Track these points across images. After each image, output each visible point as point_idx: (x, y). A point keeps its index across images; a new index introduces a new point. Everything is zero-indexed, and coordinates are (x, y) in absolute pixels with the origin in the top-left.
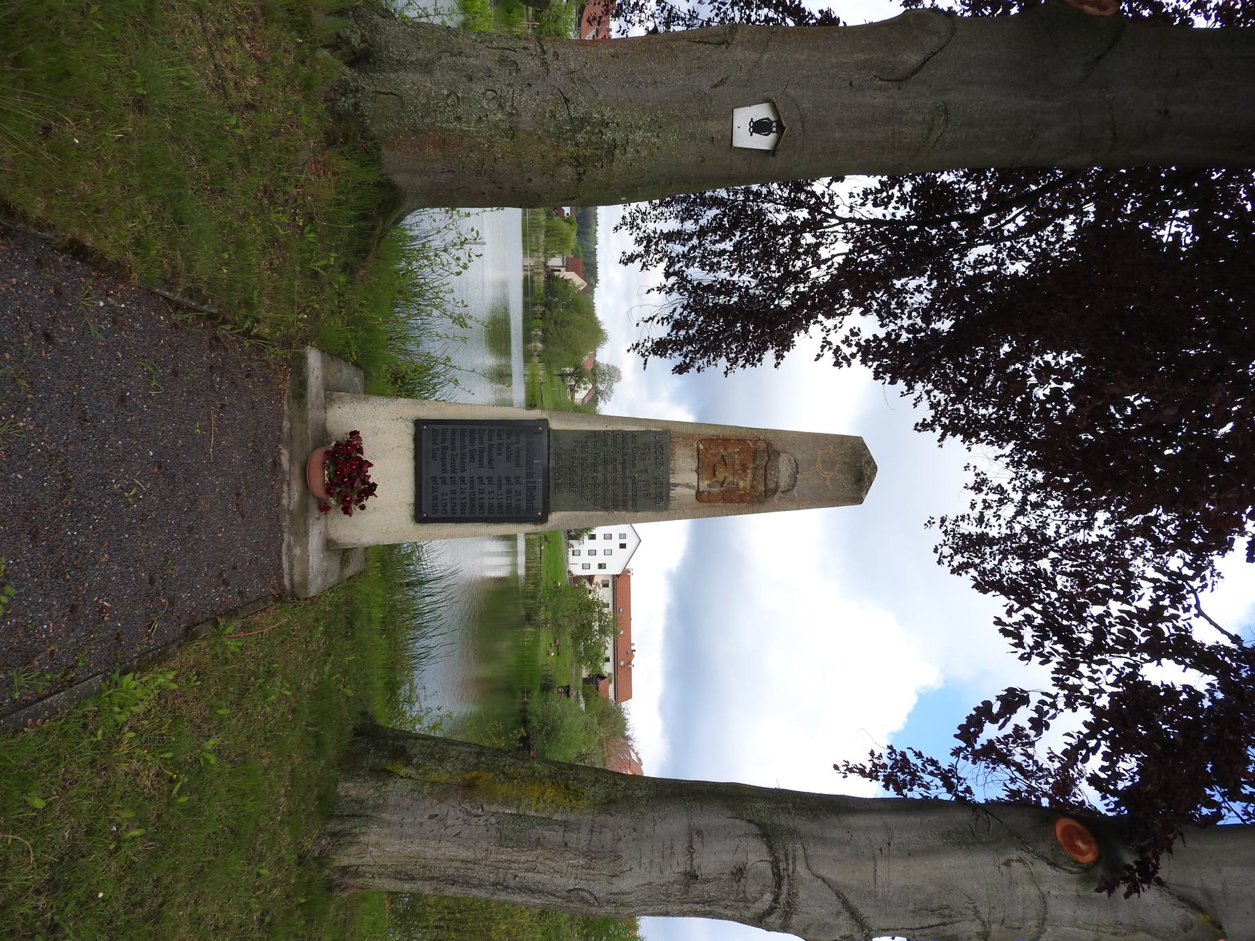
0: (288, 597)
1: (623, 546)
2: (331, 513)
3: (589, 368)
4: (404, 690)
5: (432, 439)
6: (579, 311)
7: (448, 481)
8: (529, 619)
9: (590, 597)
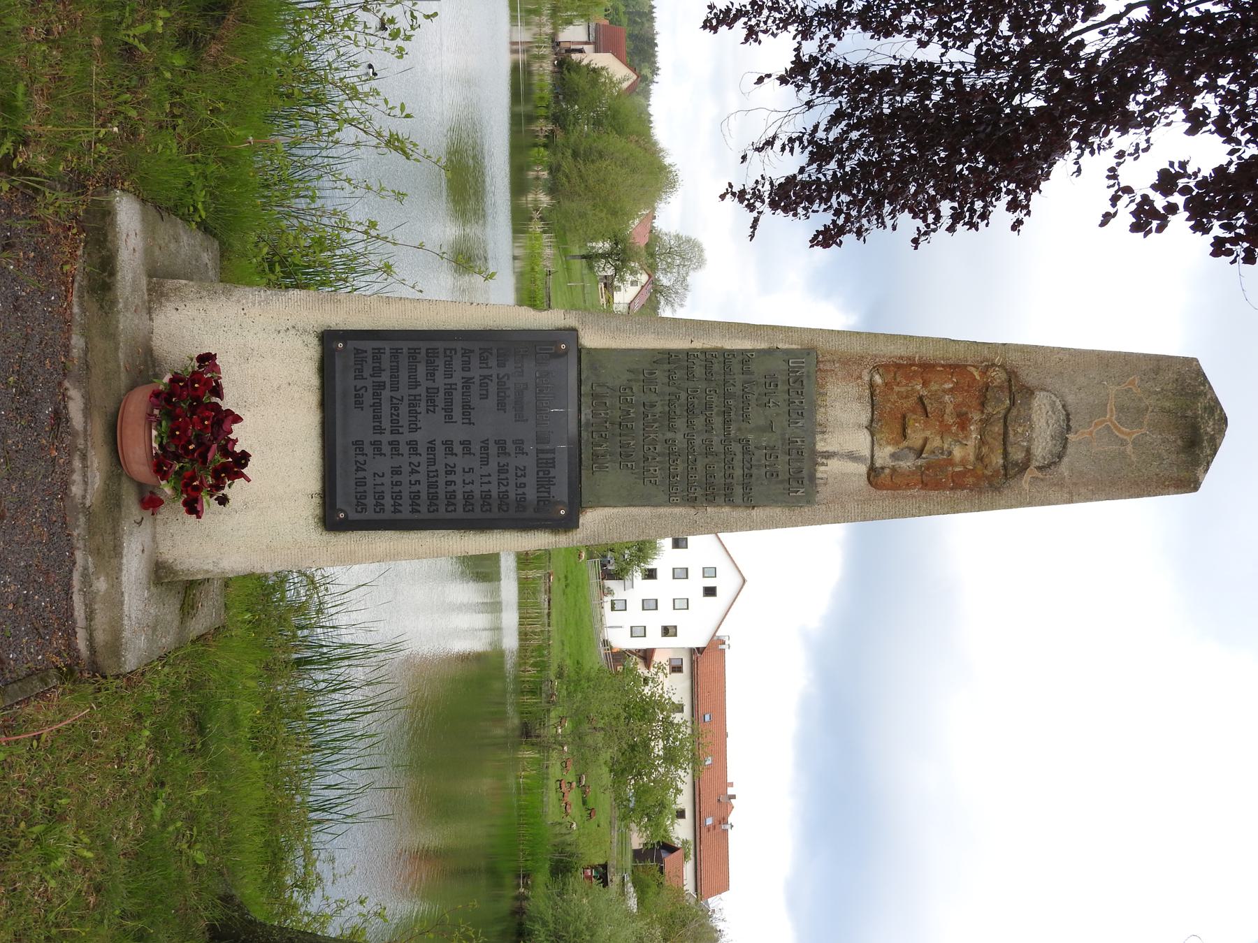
0: (86, 671)
1: (710, 592)
2: (164, 512)
3: (641, 241)
4: (297, 861)
5: (350, 364)
6: (620, 130)
7: (386, 449)
8: (527, 733)
9: (647, 690)
